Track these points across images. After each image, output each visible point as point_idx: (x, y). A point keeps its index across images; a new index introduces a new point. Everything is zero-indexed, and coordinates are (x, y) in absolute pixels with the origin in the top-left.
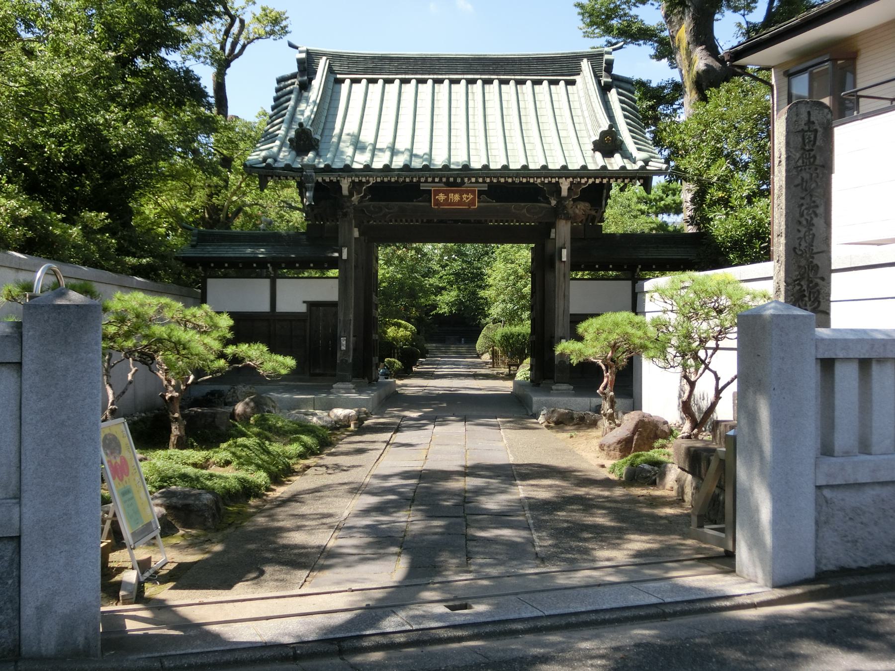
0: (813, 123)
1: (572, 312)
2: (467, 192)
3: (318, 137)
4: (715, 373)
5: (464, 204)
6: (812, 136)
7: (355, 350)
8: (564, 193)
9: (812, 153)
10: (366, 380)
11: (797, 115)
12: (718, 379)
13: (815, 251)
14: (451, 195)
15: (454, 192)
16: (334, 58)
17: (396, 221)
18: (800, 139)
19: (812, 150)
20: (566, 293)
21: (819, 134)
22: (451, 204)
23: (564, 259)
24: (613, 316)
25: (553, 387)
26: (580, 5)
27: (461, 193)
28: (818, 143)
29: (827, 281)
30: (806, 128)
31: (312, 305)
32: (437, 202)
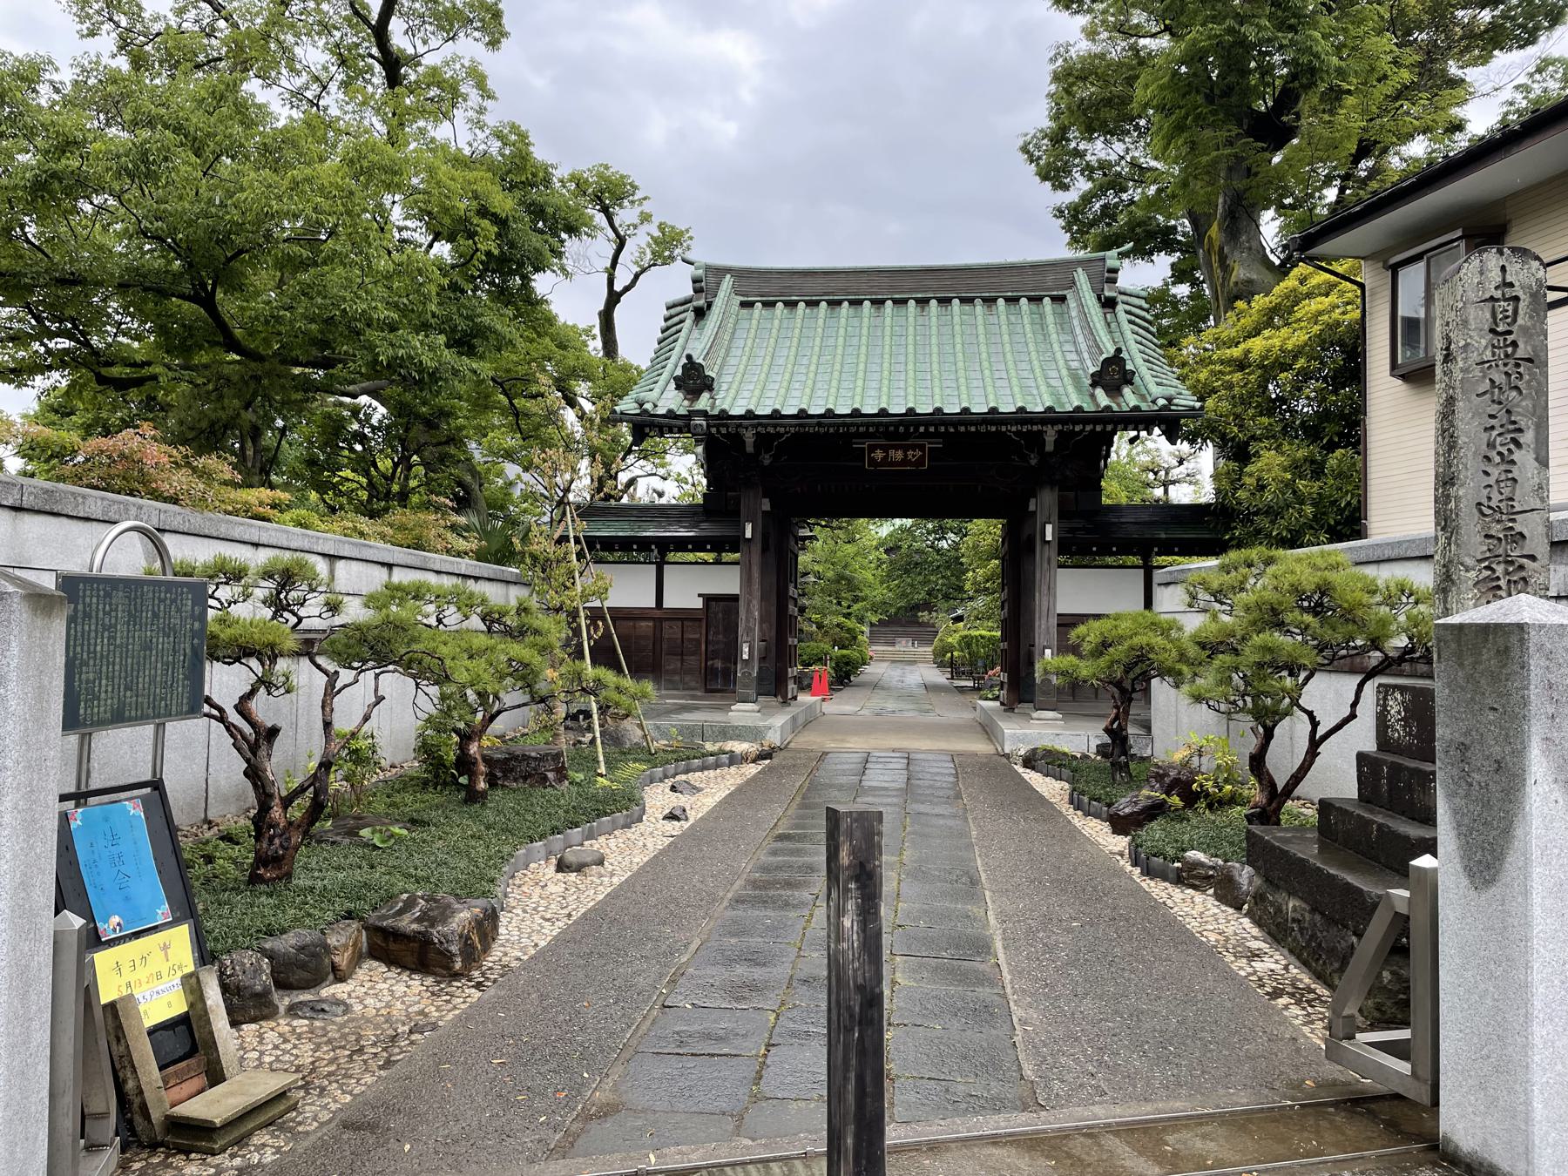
0: (1511, 285)
1: (1059, 611)
2: (914, 447)
3: (713, 375)
4: (1310, 714)
5: (909, 463)
6: (1510, 308)
7: (762, 659)
8: (1049, 447)
9: (1510, 338)
11: (1481, 273)
12: (1315, 724)
13: (1518, 509)
14: (892, 452)
15: (896, 448)
18: (1488, 315)
19: (1510, 333)
21: (1521, 304)
23: (1049, 537)
25: (1035, 715)
27: (905, 449)
28: (1520, 321)
30: (1498, 294)
31: (709, 599)
32: (872, 461)
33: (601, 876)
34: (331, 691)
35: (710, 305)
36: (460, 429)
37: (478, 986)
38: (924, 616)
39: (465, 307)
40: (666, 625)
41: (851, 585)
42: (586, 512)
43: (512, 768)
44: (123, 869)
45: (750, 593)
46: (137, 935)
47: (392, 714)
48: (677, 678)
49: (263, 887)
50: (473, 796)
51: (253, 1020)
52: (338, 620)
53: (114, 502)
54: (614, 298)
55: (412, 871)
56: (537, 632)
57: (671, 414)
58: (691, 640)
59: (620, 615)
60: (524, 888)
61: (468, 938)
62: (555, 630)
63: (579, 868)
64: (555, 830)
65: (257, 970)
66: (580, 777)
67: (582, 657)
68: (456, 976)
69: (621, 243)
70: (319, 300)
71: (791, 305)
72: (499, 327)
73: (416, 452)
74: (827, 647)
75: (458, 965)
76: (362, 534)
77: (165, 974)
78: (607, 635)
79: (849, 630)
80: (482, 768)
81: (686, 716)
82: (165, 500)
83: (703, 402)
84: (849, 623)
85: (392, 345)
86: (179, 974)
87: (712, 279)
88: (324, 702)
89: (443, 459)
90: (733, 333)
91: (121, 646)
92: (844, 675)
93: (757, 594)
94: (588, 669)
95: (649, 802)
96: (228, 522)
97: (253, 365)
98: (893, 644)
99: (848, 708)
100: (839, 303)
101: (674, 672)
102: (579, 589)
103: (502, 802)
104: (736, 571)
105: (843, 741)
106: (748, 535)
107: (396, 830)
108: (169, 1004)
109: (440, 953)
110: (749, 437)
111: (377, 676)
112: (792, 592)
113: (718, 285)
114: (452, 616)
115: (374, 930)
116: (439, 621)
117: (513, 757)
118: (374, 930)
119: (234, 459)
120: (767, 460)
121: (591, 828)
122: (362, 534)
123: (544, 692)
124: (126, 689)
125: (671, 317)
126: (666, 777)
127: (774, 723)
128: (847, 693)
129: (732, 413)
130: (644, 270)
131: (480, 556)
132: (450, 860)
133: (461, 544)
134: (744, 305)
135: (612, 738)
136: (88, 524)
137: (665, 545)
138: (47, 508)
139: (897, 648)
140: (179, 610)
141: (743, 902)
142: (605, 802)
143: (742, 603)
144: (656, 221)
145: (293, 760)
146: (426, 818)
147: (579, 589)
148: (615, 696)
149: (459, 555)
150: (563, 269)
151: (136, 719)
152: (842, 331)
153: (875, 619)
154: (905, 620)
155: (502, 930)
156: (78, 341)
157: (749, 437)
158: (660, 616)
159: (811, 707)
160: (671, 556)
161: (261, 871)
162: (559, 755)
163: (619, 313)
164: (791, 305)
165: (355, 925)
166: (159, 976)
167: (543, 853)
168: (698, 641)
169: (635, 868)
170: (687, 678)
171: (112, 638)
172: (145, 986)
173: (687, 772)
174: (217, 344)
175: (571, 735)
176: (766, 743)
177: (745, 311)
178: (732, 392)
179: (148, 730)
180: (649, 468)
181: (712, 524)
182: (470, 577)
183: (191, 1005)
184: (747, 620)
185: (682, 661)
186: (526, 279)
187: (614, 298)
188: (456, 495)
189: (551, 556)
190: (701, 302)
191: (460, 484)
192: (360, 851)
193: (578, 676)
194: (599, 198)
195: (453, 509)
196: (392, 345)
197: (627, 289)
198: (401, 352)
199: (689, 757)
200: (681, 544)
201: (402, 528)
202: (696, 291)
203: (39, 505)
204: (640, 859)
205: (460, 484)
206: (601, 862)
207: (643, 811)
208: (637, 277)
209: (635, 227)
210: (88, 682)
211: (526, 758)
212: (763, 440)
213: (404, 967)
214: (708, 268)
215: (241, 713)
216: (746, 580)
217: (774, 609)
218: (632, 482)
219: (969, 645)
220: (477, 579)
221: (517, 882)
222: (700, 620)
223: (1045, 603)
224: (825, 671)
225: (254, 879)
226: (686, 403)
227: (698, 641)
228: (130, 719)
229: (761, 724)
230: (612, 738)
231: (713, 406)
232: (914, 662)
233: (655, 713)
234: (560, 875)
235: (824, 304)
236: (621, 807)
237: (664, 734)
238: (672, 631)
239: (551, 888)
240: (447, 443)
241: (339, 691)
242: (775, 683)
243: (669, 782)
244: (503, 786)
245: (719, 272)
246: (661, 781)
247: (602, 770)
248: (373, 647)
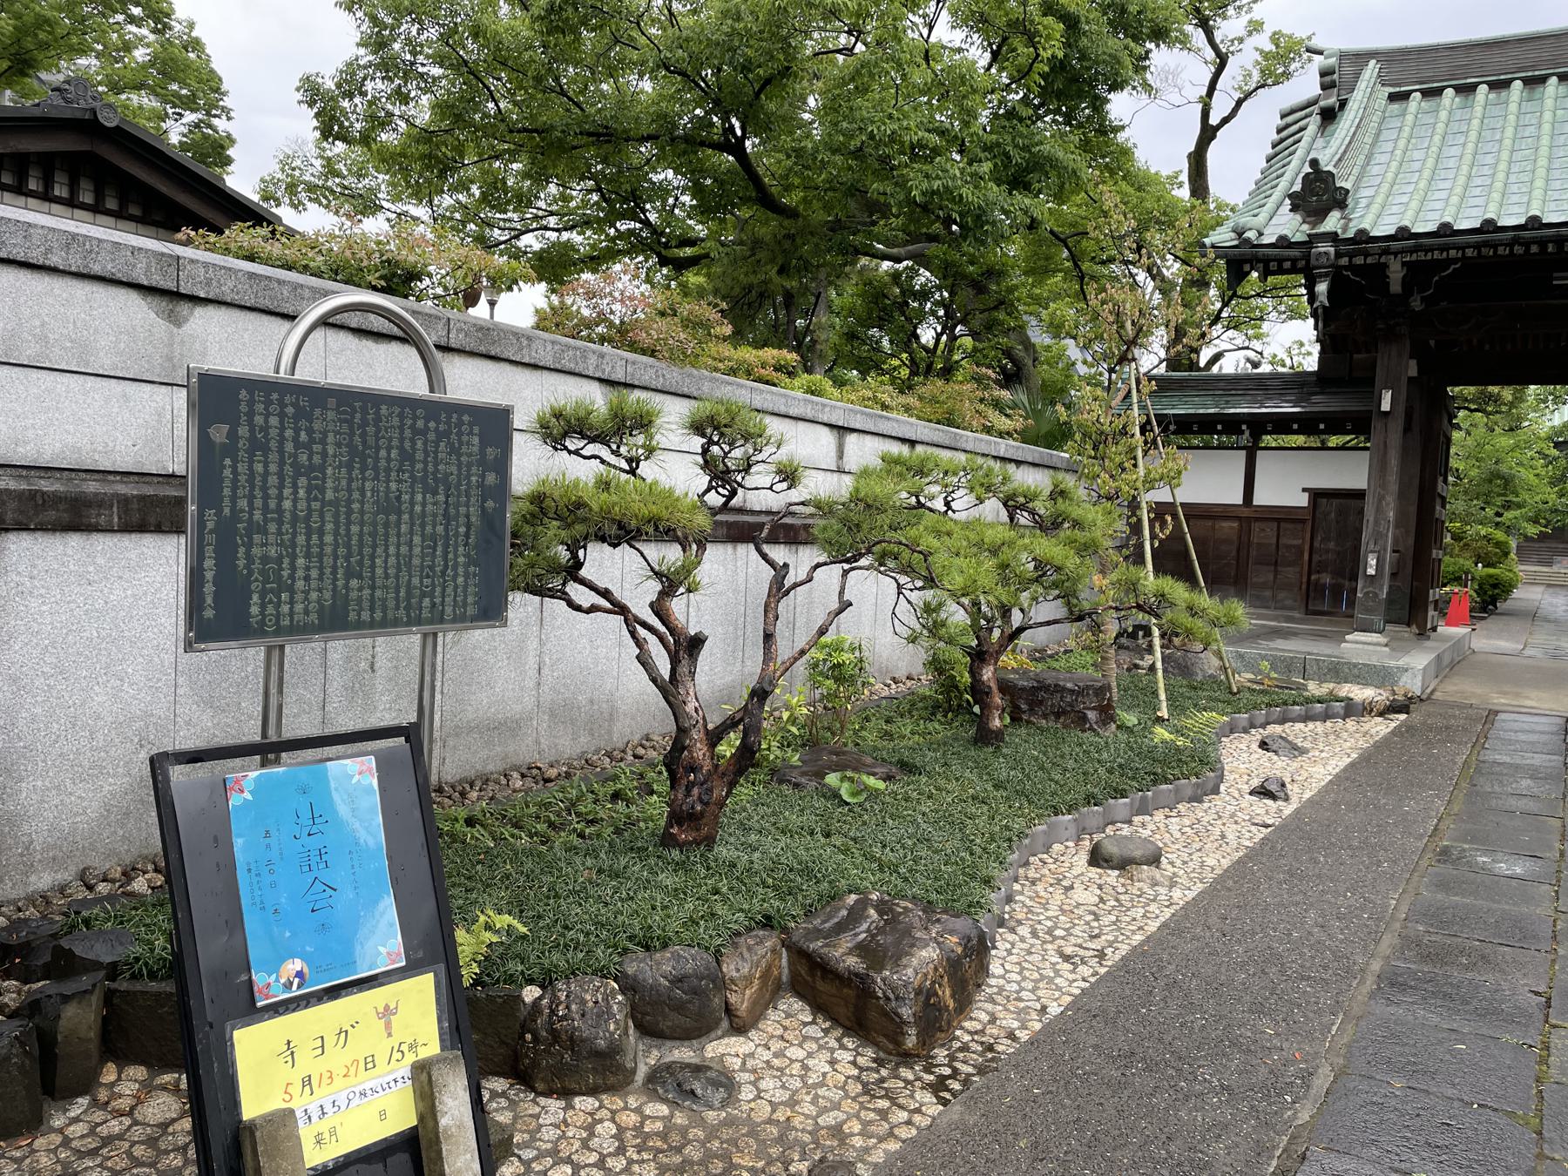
3: (1347, 185)
7: (1394, 575)
10: (1414, 629)
12: (818, 566)
16: (1392, 59)
29: (497, 325)
31: (1316, 495)
33: (1155, 884)
34: (779, 588)
35: (1343, 104)
36: (1011, 290)
37: (938, 1087)
39: (1021, 136)
40: (1256, 527)
41: (1507, 482)
42: (1164, 386)
43: (1036, 701)
44: (325, 876)
45: (1383, 486)
46: (334, 992)
47: (878, 621)
48: (1268, 593)
49: (676, 854)
50: (985, 737)
51: (593, 1091)
52: (795, 495)
53: (568, 347)
54: (1208, 133)
55: (877, 851)
56: (1077, 524)
57: (1283, 242)
58: (1288, 547)
59: (1197, 513)
60: (1040, 888)
61: (932, 993)
62: (1105, 525)
63: (1123, 864)
64: (1090, 800)
65: (604, 1014)
66: (1131, 719)
67: (1139, 559)
68: (906, 1058)
69: (1222, 61)
70: (845, 124)
71: (1466, 90)
72: (1061, 154)
73: (962, 322)
74: (1469, 564)
75: (911, 1041)
76: (885, 407)
77: (381, 1060)
78: (1177, 535)
79: (1498, 544)
80: (998, 699)
81: (1280, 644)
82: (643, 352)
83: (1332, 222)
84: (1500, 535)
85: (927, 176)
86: (410, 1058)
87: (1348, 69)
88: (766, 606)
89: (990, 326)
90: (1378, 135)
91: (335, 503)
92: (1490, 599)
93: (1394, 487)
94: (1149, 579)
95: (1229, 763)
96: (712, 380)
97: (786, 223)
98: (1549, 564)
99: (1504, 644)
102: (1141, 471)
103: (1026, 743)
105: (1517, 695)
106: (1386, 406)
107: (872, 781)
108: (383, 1115)
109: (885, 1014)
110: (1396, 272)
111: (845, 573)
113: (1357, 76)
114: (962, 501)
115: (800, 955)
116: (947, 504)
117: (1042, 687)
118: (800, 955)
119: (724, 305)
120: (1416, 304)
121: (1144, 799)
122: (885, 407)
123: (1086, 606)
124: (349, 575)
125: (1287, 126)
126: (1253, 726)
127: (1414, 666)
128: (1492, 623)
129: (1375, 233)
130: (1248, 95)
131: (1026, 437)
132: (936, 836)
133: (1004, 423)
134: (1393, 98)
135: (1179, 667)
136: (538, 373)
137: (1260, 425)
138: (482, 349)
139: (1555, 568)
140: (454, 451)
141: (1403, 987)
142: (1164, 763)
143: (1369, 499)
144: (1269, 29)
145: (719, 678)
146: (918, 761)
147: (1141, 471)
148: (1186, 620)
149: (1001, 435)
150: (1147, 87)
151: (372, 625)
152: (1548, 116)
155: (995, 968)
156: (641, 222)
157: (1396, 272)
158: (1248, 515)
159: (1459, 643)
160: (1268, 440)
161: (674, 830)
162: (1102, 690)
163: (1213, 153)
164: (1466, 90)
165: (771, 941)
166: (370, 1063)
167: (1072, 830)
169: (1210, 877)
170: (1281, 595)
171: (315, 491)
172: (339, 1082)
173: (1282, 721)
174: (749, 199)
175: (1125, 657)
176: (1400, 691)
177: (1395, 107)
178: (1375, 208)
179: (411, 641)
180: (1240, 340)
181: (1325, 405)
182: (1011, 460)
183: (421, 1118)
184: (1376, 522)
185: (1276, 572)
186: (1099, 104)
187: (1208, 133)
188: (1003, 369)
189: (1106, 428)
190: (1332, 101)
191: (1008, 353)
192: (819, 803)
193: (1132, 587)
194: (1197, 10)
195: (996, 382)
196: (927, 176)
197: (1225, 121)
198: (936, 184)
199: (1280, 703)
200: (1282, 424)
201: (934, 400)
202: (1324, 87)
203: (471, 345)
204: (1218, 861)
205: (1008, 353)
206: (1154, 860)
207: (1221, 778)
208: (1239, 103)
209: (1241, 40)
210: (265, 559)
211: (1059, 689)
212: (1417, 273)
213: (836, 1021)
214: (1343, 56)
215: (657, 614)
216: (1378, 470)
217: (1413, 509)
218: (1217, 357)
220: (1018, 463)
221: (1032, 874)
222: (1303, 521)
224: (1466, 593)
225: (667, 840)
226: (1305, 227)
228: (359, 625)
229: (1393, 663)
230: (1179, 667)
231: (1345, 229)
233: (1238, 637)
234: (1094, 872)
235: (1518, 84)
236: (1192, 771)
237: (1252, 666)
238: (1264, 535)
239: (1079, 895)
240: (996, 308)
241: (787, 593)
242: (1411, 608)
243: (1258, 734)
244: (1028, 722)
245: (1359, 58)
246: (1246, 731)
247: (1164, 713)
248: (857, 532)
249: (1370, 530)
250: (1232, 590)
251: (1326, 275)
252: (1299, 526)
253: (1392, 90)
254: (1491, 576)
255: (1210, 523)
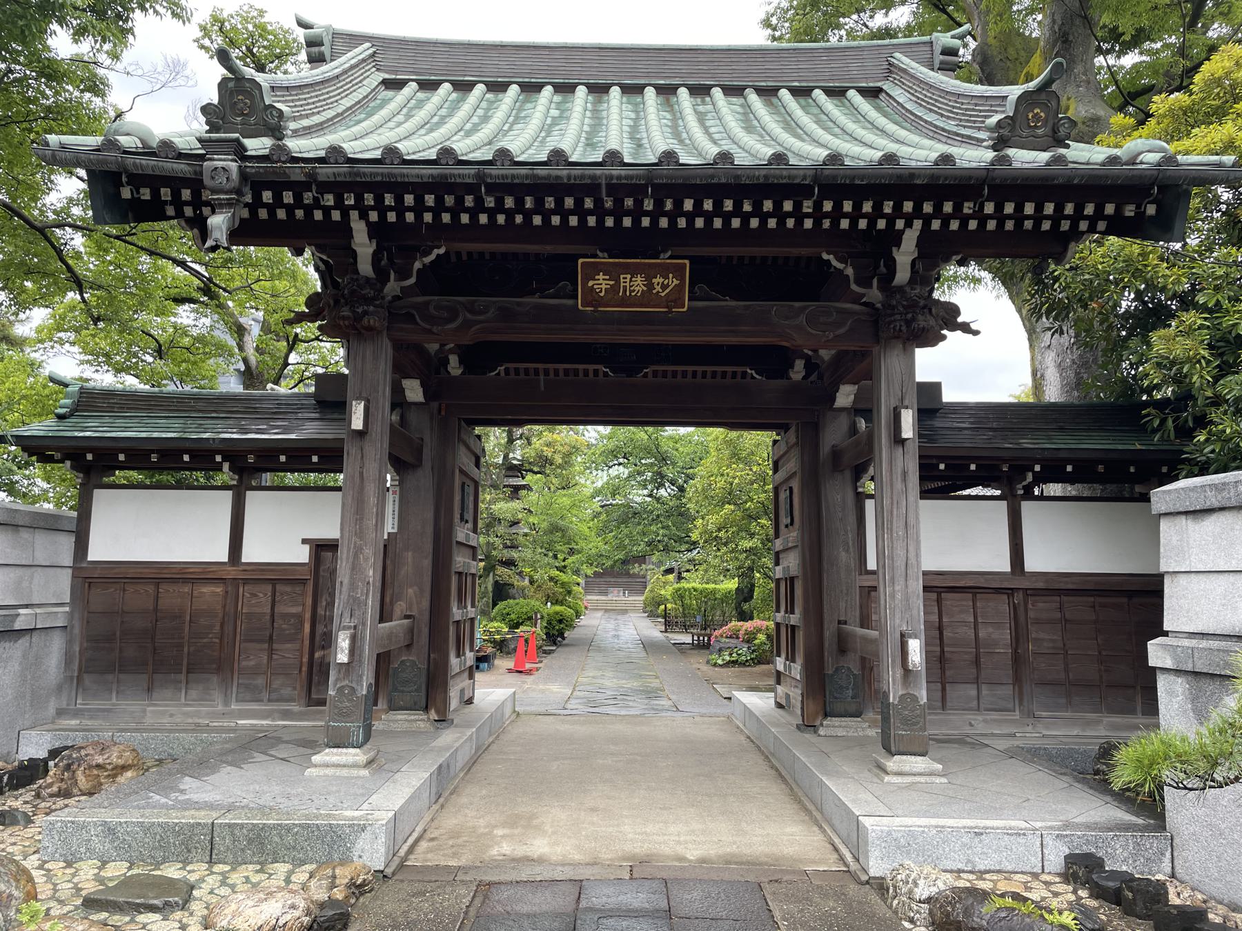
1: (924, 568)
5: (606, 270)
14: (625, 279)
15: (634, 271)
16: (383, 45)
17: (586, 373)
20: (911, 521)
22: (624, 302)
24: (615, 138)
25: (893, 763)
26: (966, 328)
32: (592, 298)
38: (636, 569)
45: (360, 534)
48: (260, 681)
71: (463, 87)
79: (563, 584)
84: (563, 577)
98: (606, 594)
100: (538, 88)
101: (255, 672)
104: (334, 500)
112: (462, 533)
139: (610, 597)
143: (343, 553)
153: (589, 572)
154: (619, 572)
158: (236, 575)
168: (300, 618)
170: (277, 683)
184: (353, 586)
185: (271, 651)
219: (681, 597)
222: (303, 582)
223: (900, 552)
227: (300, 618)
232: (624, 612)
238: (257, 602)
249: (344, 596)
250: (215, 679)
251: (229, 204)
252: (298, 589)
253: (387, 76)
254: (557, 613)
255: (187, 589)
